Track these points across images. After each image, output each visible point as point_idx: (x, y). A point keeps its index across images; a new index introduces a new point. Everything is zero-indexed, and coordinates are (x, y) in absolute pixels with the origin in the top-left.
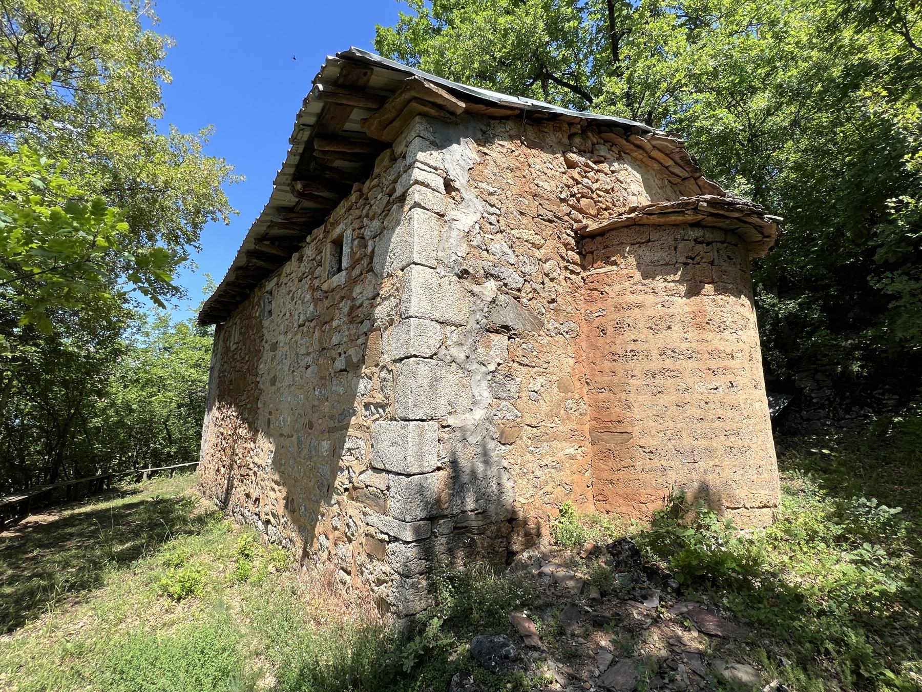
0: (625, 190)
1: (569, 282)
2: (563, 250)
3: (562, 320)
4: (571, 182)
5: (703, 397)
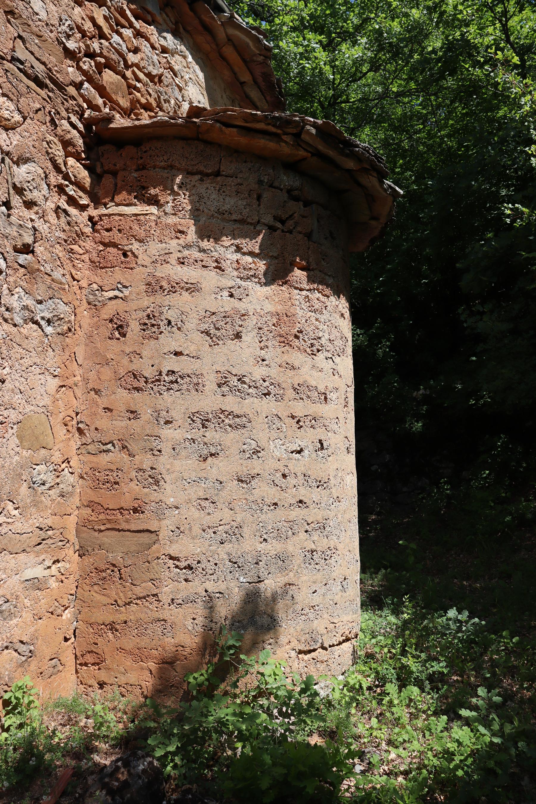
0: (180, 89)
1: (63, 219)
2: (58, 151)
3: (41, 292)
4: (88, 26)
5: (280, 466)
